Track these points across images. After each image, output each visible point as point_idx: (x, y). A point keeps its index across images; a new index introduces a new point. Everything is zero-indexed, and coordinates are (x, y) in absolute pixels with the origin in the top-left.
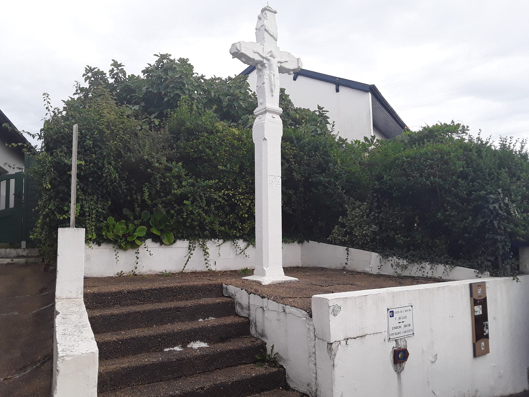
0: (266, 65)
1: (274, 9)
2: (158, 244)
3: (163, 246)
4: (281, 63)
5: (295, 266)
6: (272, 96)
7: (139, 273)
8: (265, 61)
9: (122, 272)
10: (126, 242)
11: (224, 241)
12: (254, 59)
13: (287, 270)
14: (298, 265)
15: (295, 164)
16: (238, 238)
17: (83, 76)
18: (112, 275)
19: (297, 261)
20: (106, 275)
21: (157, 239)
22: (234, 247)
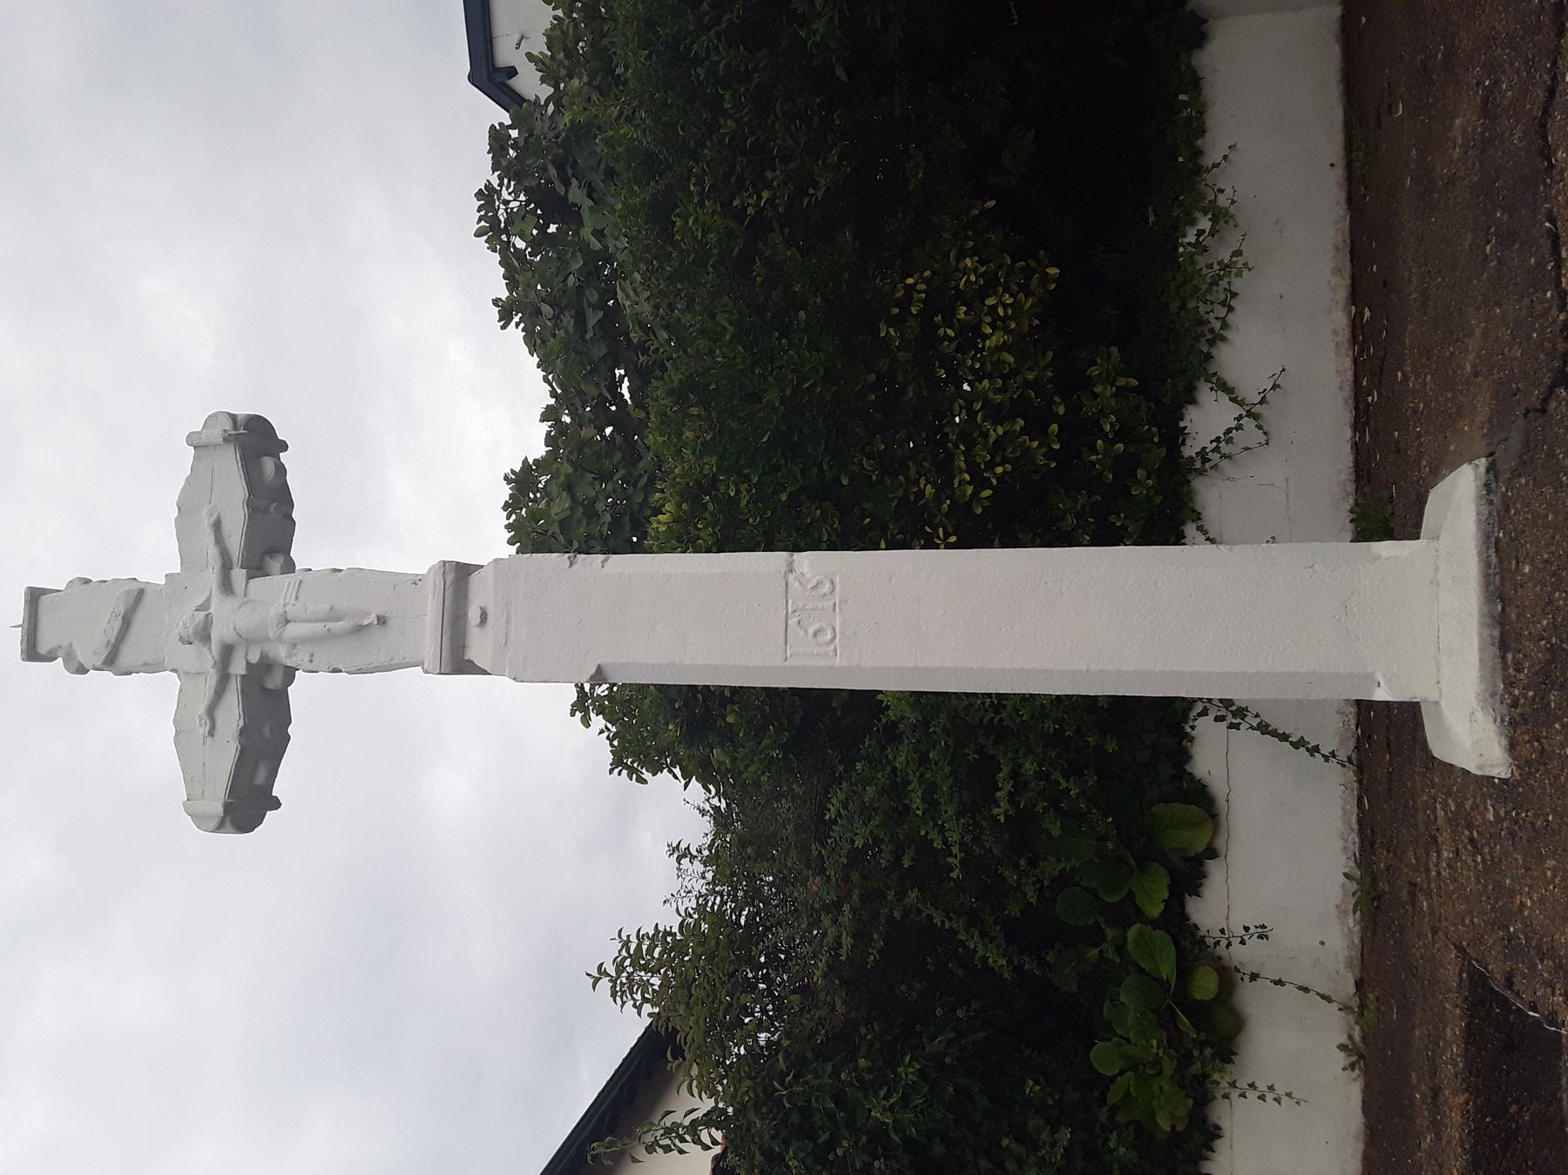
0: (254, 658)
1: (18, 612)
2: (1212, 866)
3: (1220, 843)
4: (226, 566)
5: (1335, 52)
6: (382, 621)
7: (1349, 965)
8: (238, 668)
9: (1342, 1047)
10: (1202, 1022)
11: (1197, 517)
12: (243, 733)
13: (1384, 507)
14: (1335, 26)
15: (768, 185)
16: (1175, 436)
17: (644, 782)
18: (1355, 1092)
19: (1316, 435)
20: (1356, 1119)
21: (1189, 877)
22: (1224, 464)
